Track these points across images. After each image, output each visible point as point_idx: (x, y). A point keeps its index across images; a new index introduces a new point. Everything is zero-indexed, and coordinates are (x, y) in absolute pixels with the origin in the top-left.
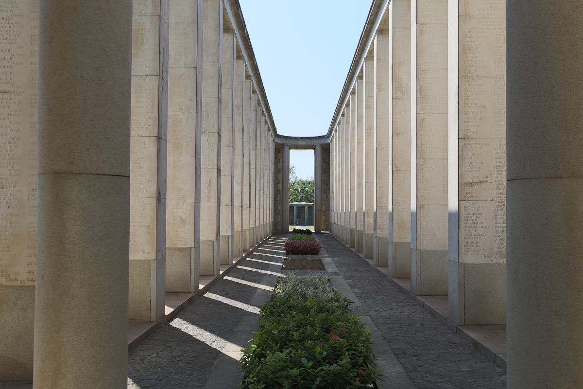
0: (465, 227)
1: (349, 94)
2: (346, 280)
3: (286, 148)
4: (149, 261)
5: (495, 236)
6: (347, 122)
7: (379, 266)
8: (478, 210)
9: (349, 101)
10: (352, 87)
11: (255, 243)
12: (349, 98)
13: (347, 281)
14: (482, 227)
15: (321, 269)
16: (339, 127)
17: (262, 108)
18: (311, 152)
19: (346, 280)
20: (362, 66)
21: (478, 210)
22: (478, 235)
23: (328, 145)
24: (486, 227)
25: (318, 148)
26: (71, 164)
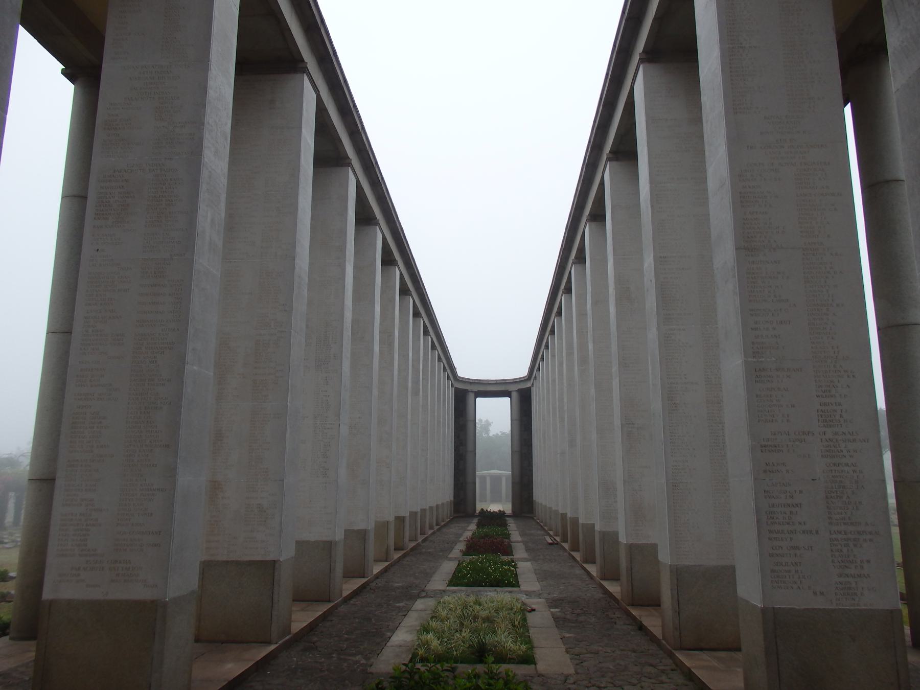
0: (770, 532)
1: (605, 157)
2: (550, 607)
3: (472, 396)
4: (153, 602)
5: (832, 551)
6: (553, 356)
7: (633, 605)
8: (792, 497)
9: (536, 377)
10: (624, 100)
11: (392, 548)
12: (548, 338)
13: (552, 610)
14: (804, 532)
15: (513, 586)
16: (553, 340)
17: (432, 339)
18: (507, 400)
19: (550, 607)
20: (570, 273)
21: (792, 497)
22: (797, 548)
23: (529, 390)
24: (811, 532)
25: (514, 395)
26: (549, 594)
